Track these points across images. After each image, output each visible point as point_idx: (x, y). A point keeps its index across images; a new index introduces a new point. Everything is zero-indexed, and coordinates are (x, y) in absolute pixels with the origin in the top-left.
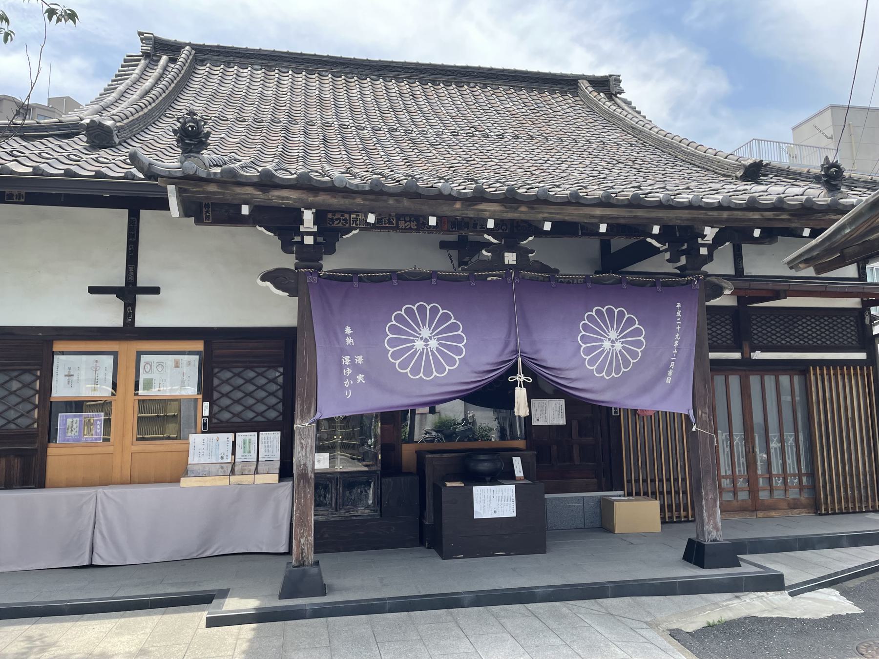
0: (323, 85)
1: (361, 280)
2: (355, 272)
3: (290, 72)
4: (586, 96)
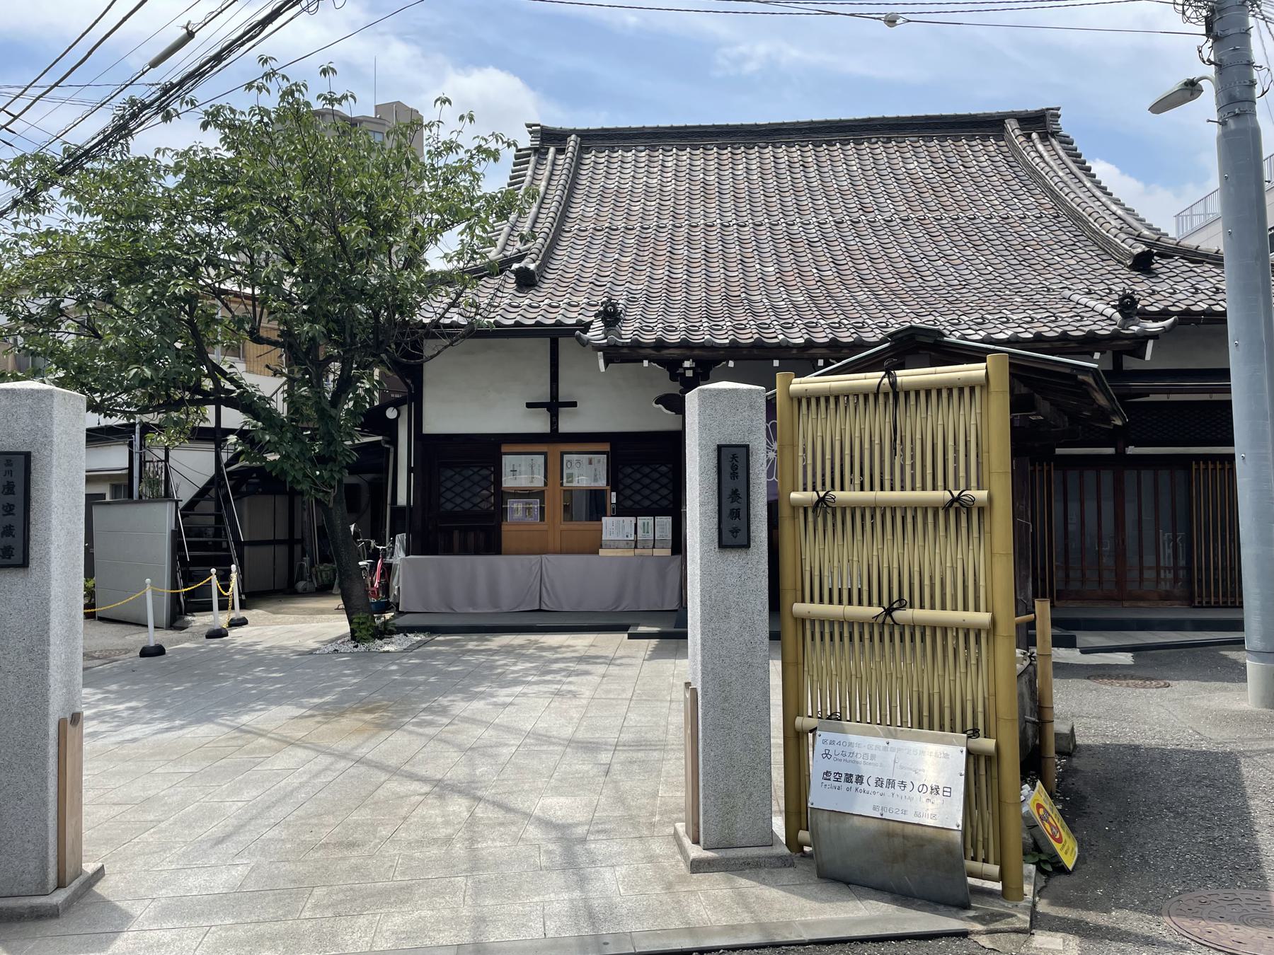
4: (1011, 142)
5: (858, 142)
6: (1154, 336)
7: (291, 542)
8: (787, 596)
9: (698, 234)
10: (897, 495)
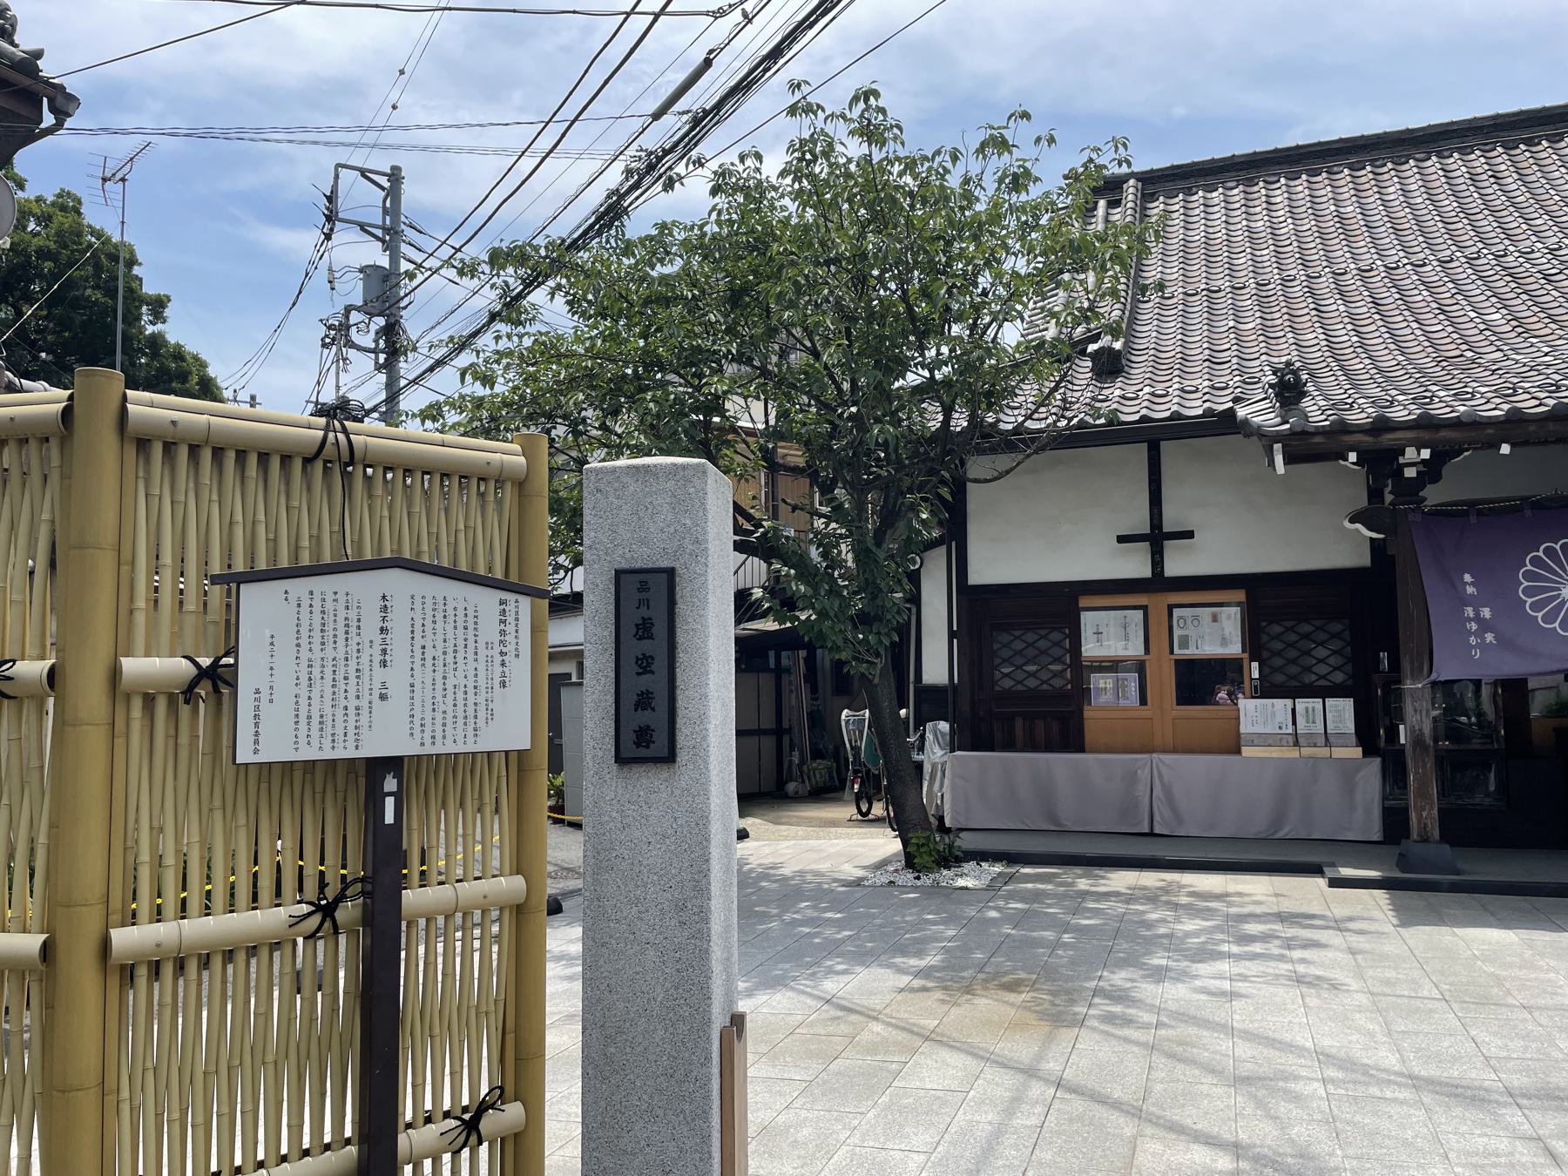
0: (1336, 191)
1: (1480, 513)
2: (1472, 504)
3: (1283, 181)
7: (779, 732)
9: (1352, 282)
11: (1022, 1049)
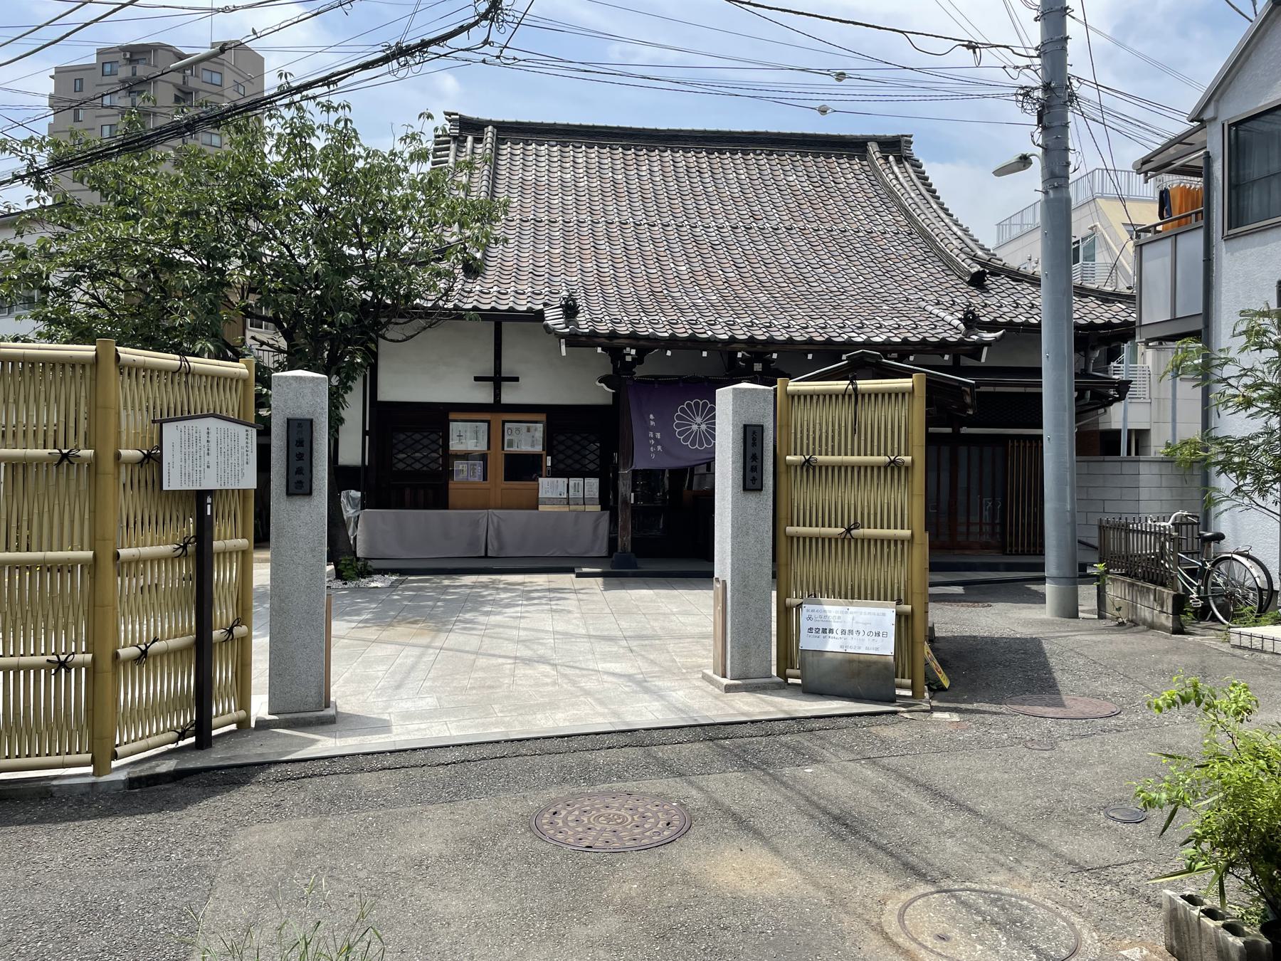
0: (612, 160)
1: (660, 383)
2: (656, 377)
4: (873, 163)
5: (745, 153)
6: (988, 344)
8: (782, 523)
10: (856, 458)
11: (425, 640)
